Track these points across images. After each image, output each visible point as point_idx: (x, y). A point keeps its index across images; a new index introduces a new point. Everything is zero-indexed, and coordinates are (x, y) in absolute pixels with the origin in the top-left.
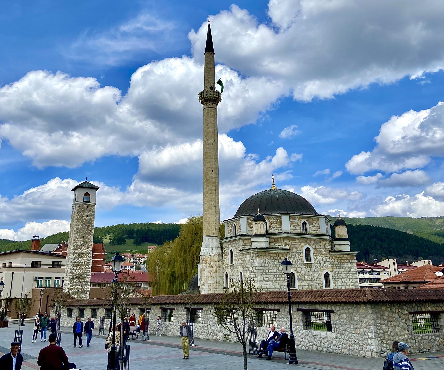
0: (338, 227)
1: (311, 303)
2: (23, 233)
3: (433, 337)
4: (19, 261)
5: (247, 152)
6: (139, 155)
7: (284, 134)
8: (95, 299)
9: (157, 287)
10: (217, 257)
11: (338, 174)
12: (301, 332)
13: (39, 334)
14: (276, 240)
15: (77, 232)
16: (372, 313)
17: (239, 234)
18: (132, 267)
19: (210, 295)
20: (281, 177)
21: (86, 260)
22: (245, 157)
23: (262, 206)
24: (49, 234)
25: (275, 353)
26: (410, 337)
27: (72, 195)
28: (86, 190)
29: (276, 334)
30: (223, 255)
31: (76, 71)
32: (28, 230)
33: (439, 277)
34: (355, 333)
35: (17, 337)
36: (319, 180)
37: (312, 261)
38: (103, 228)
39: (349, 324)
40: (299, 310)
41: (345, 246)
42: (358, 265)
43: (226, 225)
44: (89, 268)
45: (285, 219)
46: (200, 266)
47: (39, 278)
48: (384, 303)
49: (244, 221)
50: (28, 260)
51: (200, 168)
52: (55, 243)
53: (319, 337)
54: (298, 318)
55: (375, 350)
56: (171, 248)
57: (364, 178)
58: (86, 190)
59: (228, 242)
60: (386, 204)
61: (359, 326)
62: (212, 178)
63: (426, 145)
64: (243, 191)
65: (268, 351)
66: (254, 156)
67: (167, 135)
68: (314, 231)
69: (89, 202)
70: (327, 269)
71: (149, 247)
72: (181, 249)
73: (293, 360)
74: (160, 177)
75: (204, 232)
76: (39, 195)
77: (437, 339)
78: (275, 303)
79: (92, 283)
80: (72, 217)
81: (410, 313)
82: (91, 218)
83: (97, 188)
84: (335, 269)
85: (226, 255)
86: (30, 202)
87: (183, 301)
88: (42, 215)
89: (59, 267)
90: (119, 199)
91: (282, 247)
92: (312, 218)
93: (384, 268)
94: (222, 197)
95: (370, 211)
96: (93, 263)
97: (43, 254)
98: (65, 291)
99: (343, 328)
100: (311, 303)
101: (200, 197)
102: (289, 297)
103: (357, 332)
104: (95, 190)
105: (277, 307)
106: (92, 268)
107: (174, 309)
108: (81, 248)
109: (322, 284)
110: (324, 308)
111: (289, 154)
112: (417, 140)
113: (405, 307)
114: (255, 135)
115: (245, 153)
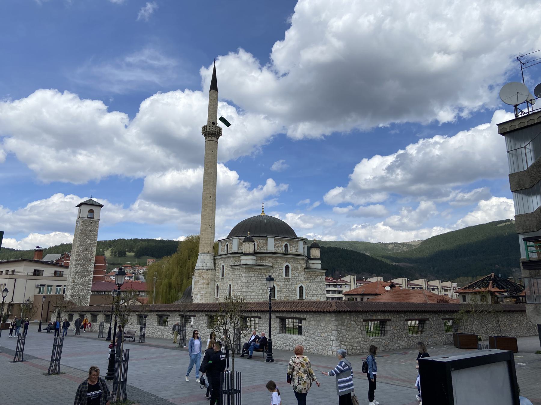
0: (313, 249)
1: (287, 312)
2: (26, 243)
3: (381, 340)
4: (21, 269)
5: (239, 179)
6: (145, 177)
7: (276, 166)
8: (95, 305)
9: (154, 295)
10: (210, 272)
11: (317, 204)
12: (278, 335)
13: (14, 331)
14: (262, 259)
15: (80, 245)
16: (335, 320)
17: (230, 252)
18: (132, 277)
19: (202, 304)
20: (270, 204)
21: (88, 271)
22: (239, 184)
23: (253, 229)
24: (52, 245)
25: (255, 353)
26: (363, 340)
27: (76, 210)
28: (91, 207)
29: (257, 337)
30: (215, 269)
31: (85, 93)
32: (31, 240)
33: (387, 291)
34: (321, 336)
35: (56, 346)
36: (302, 209)
37: (290, 277)
38: (105, 241)
39: (317, 329)
40: (277, 317)
41: (317, 265)
42: (326, 279)
43: (220, 244)
44: (91, 277)
45: (271, 241)
46: (194, 279)
47: (41, 285)
48: (345, 312)
49: (235, 241)
50: (31, 268)
51: (200, 193)
52: (58, 253)
53: (292, 339)
54: (276, 324)
55: (335, 350)
56: (168, 262)
57: (338, 209)
58: (91, 207)
59: (221, 258)
60: (354, 230)
61: (324, 331)
62: (210, 203)
63: (388, 184)
64: (236, 214)
65: (250, 352)
66: (246, 184)
67: (172, 160)
68: (294, 252)
69: (93, 218)
70: (302, 283)
71: (148, 260)
72: (178, 263)
73: (270, 359)
74: (163, 198)
75: (200, 250)
76: (43, 208)
77: (384, 341)
78: (257, 311)
79: (92, 291)
80: (76, 232)
81: (364, 321)
82: (94, 232)
83: (102, 206)
84: (308, 283)
85: (218, 270)
86: (35, 215)
87: (177, 309)
88: (46, 227)
89: (61, 276)
90: (122, 216)
91: (267, 264)
92: (293, 241)
93: (346, 282)
94: (219, 219)
95: (341, 235)
96: (95, 273)
97: (45, 263)
98: (68, 297)
99: (311, 332)
100: (287, 312)
101: (198, 217)
102: (270, 308)
103: (322, 336)
104: (99, 208)
105: (259, 315)
106: (94, 277)
107: (169, 316)
108: (83, 260)
109: (297, 295)
110: (298, 316)
111: (278, 184)
112: (383, 179)
113: (361, 316)
114: (250, 166)
115: (238, 180)
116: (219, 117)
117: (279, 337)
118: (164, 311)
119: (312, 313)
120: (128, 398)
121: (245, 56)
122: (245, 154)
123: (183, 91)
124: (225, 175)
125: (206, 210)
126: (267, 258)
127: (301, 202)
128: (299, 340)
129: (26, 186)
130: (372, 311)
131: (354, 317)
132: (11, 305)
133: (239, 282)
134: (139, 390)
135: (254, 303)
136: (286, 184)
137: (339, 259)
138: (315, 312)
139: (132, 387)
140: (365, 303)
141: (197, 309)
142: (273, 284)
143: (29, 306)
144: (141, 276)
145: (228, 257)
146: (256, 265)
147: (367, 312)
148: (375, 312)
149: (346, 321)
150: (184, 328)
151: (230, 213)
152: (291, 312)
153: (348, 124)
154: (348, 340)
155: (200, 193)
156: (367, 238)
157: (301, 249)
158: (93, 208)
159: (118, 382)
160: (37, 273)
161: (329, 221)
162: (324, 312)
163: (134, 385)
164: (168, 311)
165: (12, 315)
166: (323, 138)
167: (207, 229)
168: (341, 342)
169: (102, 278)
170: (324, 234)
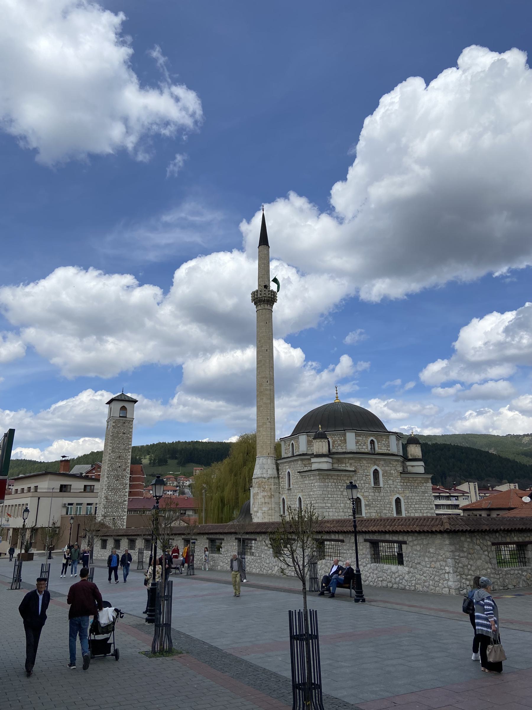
0: (411, 446)
2: (51, 453)
3: (520, 572)
4: (45, 484)
5: (307, 360)
8: (133, 528)
9: (203, 514)
10: (272, 481)
12: (369, 566)
14: (339, 461)
15: (112, 452)
16: (450, 544)
17: (297, 453)
18: (176, 491)
19: (264, 524)
20: (345, 389)
21: (122, 484)
23: (326, 421)
24: (81, 454)
25: (339, 590)
26: (494, 571)
27: (106, 409)
28: (122, 403)
29: (340, 568)
33: (526, 503)
34: (430, 567)
38: (142, 446)
40: (366, 540)
41: (419, 467)
42: (433, 489)
43: (282, 443)
44: (126, 492)
45: (351, 436)
46: (253, 491)
47: (69, 504)
49: (303, 439)
50: (56, 483)
53: (389, 571)
54: (365, 549)
55: (453, 587)
57: (440, 390)
59: (285, 462)
60: (465, 419)
61: (435, 559)
64: (302, 405)
65: (331, 588)
67: (215, 340)
69: (126, 417)
70: (399, 493)
71: (195, 468)
72: (231, 471)
73: (360, 598)
74: (208, 389)
76: (68, 409)
78: (338, 533)
79: (129, 510)
80: (107, 435)
81: (493, 544)
82: (128, 435)
83: (135, 401)
84: (408, 493)
85: (282, 478)
86: (58, 418)
87: (233, 531)
92: (381, 436)
93: (464, 493)
94: (279, 412)
95: (448, 427)
96: (131, 486)
97: (74, 476)
98: (99, 519)
99: (416, 561)
101: (253, 411)
102: (355, 526)
103: (433, 566)
104: (132, 404)
105: (341, 537)
106: (130, 492)
107: (223, 539)
108: (117, 470)
111: (355, 362)
112: (501, 346)
113: (487, 537)
116: (271, 279)
117: (371, 568)
118: (216, 533)
119: (416, 534)
120: (174, 647)
121: (298, 202)
122: (308, 327)
123: (231, 252)
124: (285, 353)
125: (262, 399)
126: (347, 460)
127: (387, 383)
129: (44, 384)
130: (504, 530)
132: (34, 530)
134: (188, 636)
137: (450, 460)
139: (178, 632)
140: (494, 519)
141: (258, 530)
143: (56, 531)
144: (187, 490)
145: (295, 460)
147: (496, 531)
148: (509, 531)
149: (466, 545)
150: (243, 556)
151: (295, 403)
152: (385, 532)
153: (441, 276)
154: (471, 572)
155: (253, 378)
156: (487, 428)
157: (394, 447)
159: (160, 624)
160: (64, 489)
161: (430, 407)
162: (432, 532)
163: (182, 630)
164: (221, 533)
165: (35, 543)
166: (405, 297)
167: (265, 423)
168: (461, 575)
169: (140, 494)
170: (426, 427)
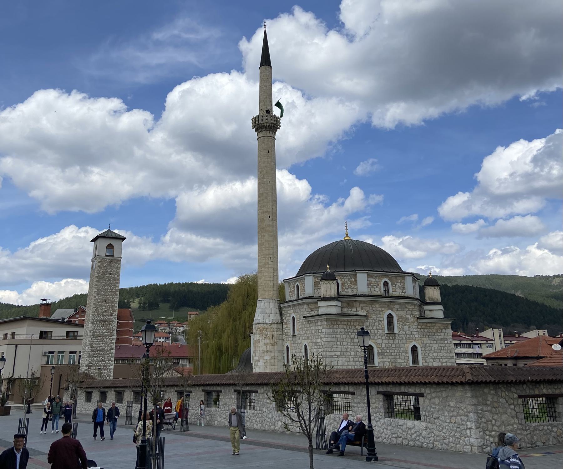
0: (429, 288)
2: (29, 296)
3: (550, 427)
4: (23, 331)
5: (313, 192)
9: (199, 364)
10: (275, 326)
12: (382, 421)
14: (350, 305)
15: (98, 294)
17: (303, 296)
18: (168, 338)
19: (266, 374)
20: (355, 225)
21: (109, 330)
22: (311, 199)
24: (63, 297)
25: (349, 448)
26: (520, 427)
27: (91, 247)
28: (109, 241)
29: (350, 423)
30: (282, 323)
33: (557, 351)
36: (404, 229)
37: (396, 331)
38: (131, 289)
40: (379, 393)
41: (438, 312)
42: (453, 336)
43: (286, 285)
44: (113, 339)
45: (362, 277)
47: (50, 353)
48: (487, 383)
49: (309, 280)
50: (35, 329)
52: (70, 307)
53: (405, 427)
54: (378, 403)
56: (217, 314)
57: (461, 226)
59: (290, 306)
61: (455, 413)
63: (540, 184)
64: (307, 243)
65: (340, 446)
66: (322, 197)
67: (212, 171)
68: (399, 293)
69: (113, 256)
70: (415, 341)
71: (189, 313)
72: (229, 316)
73: (372, 456)
74: (203, 225)
76: (49, 247)
78: (348, 384)
79: (116, 359)
80: (92, 276)
81: (520, 397)
82: (115, 276)
83: (123, 239)
84: (425, 340)
85: (286, 323)
87: (231, 382)
89: (75, 338)
91: (359, 313)
92: (396, 277)
93: (487, 340)
94: (282, 251)
95: (470, 267)
96: (118, 333)
97: (55, 321)
98: (83, 369)
99: (434, 416)
101: (254, 250)
102: (367, 377)
104: (120, 241)
105: (351, 389)
106: (117, 339)
107: (221, 392)
108: (103, 315)
109: (408, 360)
111: (367, 194)
112: (529, 177)
113: (513, 389)
115: (311, 194)
116: (274, 103)
121: (304, 17)
122: (315, 156)
124: (290, 186)
125: (264, 236)
127: (403, 219)
128: (417, 428)
129: (35, 220)
130: (532, 381)
131: (502, 391)
133: (319, 340)
135: (343, 371)
136: (379, 194)
137: (472, 304)
138: (438, 384)
142: (369, 341)
145: (300, 304)
146: (342, 314)
147: (524, 383)
148: (537, 383)
150: (243, 410)
152: (401, 384)
156: (513, 268)
157: (411, 289)
158: (113, 242)
161: (450, 246)
162: (452, 384)
164: (218, 385)
166: (423, 123)
167: (266, 263)
